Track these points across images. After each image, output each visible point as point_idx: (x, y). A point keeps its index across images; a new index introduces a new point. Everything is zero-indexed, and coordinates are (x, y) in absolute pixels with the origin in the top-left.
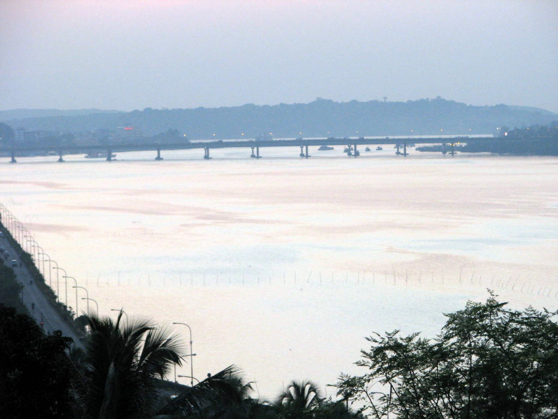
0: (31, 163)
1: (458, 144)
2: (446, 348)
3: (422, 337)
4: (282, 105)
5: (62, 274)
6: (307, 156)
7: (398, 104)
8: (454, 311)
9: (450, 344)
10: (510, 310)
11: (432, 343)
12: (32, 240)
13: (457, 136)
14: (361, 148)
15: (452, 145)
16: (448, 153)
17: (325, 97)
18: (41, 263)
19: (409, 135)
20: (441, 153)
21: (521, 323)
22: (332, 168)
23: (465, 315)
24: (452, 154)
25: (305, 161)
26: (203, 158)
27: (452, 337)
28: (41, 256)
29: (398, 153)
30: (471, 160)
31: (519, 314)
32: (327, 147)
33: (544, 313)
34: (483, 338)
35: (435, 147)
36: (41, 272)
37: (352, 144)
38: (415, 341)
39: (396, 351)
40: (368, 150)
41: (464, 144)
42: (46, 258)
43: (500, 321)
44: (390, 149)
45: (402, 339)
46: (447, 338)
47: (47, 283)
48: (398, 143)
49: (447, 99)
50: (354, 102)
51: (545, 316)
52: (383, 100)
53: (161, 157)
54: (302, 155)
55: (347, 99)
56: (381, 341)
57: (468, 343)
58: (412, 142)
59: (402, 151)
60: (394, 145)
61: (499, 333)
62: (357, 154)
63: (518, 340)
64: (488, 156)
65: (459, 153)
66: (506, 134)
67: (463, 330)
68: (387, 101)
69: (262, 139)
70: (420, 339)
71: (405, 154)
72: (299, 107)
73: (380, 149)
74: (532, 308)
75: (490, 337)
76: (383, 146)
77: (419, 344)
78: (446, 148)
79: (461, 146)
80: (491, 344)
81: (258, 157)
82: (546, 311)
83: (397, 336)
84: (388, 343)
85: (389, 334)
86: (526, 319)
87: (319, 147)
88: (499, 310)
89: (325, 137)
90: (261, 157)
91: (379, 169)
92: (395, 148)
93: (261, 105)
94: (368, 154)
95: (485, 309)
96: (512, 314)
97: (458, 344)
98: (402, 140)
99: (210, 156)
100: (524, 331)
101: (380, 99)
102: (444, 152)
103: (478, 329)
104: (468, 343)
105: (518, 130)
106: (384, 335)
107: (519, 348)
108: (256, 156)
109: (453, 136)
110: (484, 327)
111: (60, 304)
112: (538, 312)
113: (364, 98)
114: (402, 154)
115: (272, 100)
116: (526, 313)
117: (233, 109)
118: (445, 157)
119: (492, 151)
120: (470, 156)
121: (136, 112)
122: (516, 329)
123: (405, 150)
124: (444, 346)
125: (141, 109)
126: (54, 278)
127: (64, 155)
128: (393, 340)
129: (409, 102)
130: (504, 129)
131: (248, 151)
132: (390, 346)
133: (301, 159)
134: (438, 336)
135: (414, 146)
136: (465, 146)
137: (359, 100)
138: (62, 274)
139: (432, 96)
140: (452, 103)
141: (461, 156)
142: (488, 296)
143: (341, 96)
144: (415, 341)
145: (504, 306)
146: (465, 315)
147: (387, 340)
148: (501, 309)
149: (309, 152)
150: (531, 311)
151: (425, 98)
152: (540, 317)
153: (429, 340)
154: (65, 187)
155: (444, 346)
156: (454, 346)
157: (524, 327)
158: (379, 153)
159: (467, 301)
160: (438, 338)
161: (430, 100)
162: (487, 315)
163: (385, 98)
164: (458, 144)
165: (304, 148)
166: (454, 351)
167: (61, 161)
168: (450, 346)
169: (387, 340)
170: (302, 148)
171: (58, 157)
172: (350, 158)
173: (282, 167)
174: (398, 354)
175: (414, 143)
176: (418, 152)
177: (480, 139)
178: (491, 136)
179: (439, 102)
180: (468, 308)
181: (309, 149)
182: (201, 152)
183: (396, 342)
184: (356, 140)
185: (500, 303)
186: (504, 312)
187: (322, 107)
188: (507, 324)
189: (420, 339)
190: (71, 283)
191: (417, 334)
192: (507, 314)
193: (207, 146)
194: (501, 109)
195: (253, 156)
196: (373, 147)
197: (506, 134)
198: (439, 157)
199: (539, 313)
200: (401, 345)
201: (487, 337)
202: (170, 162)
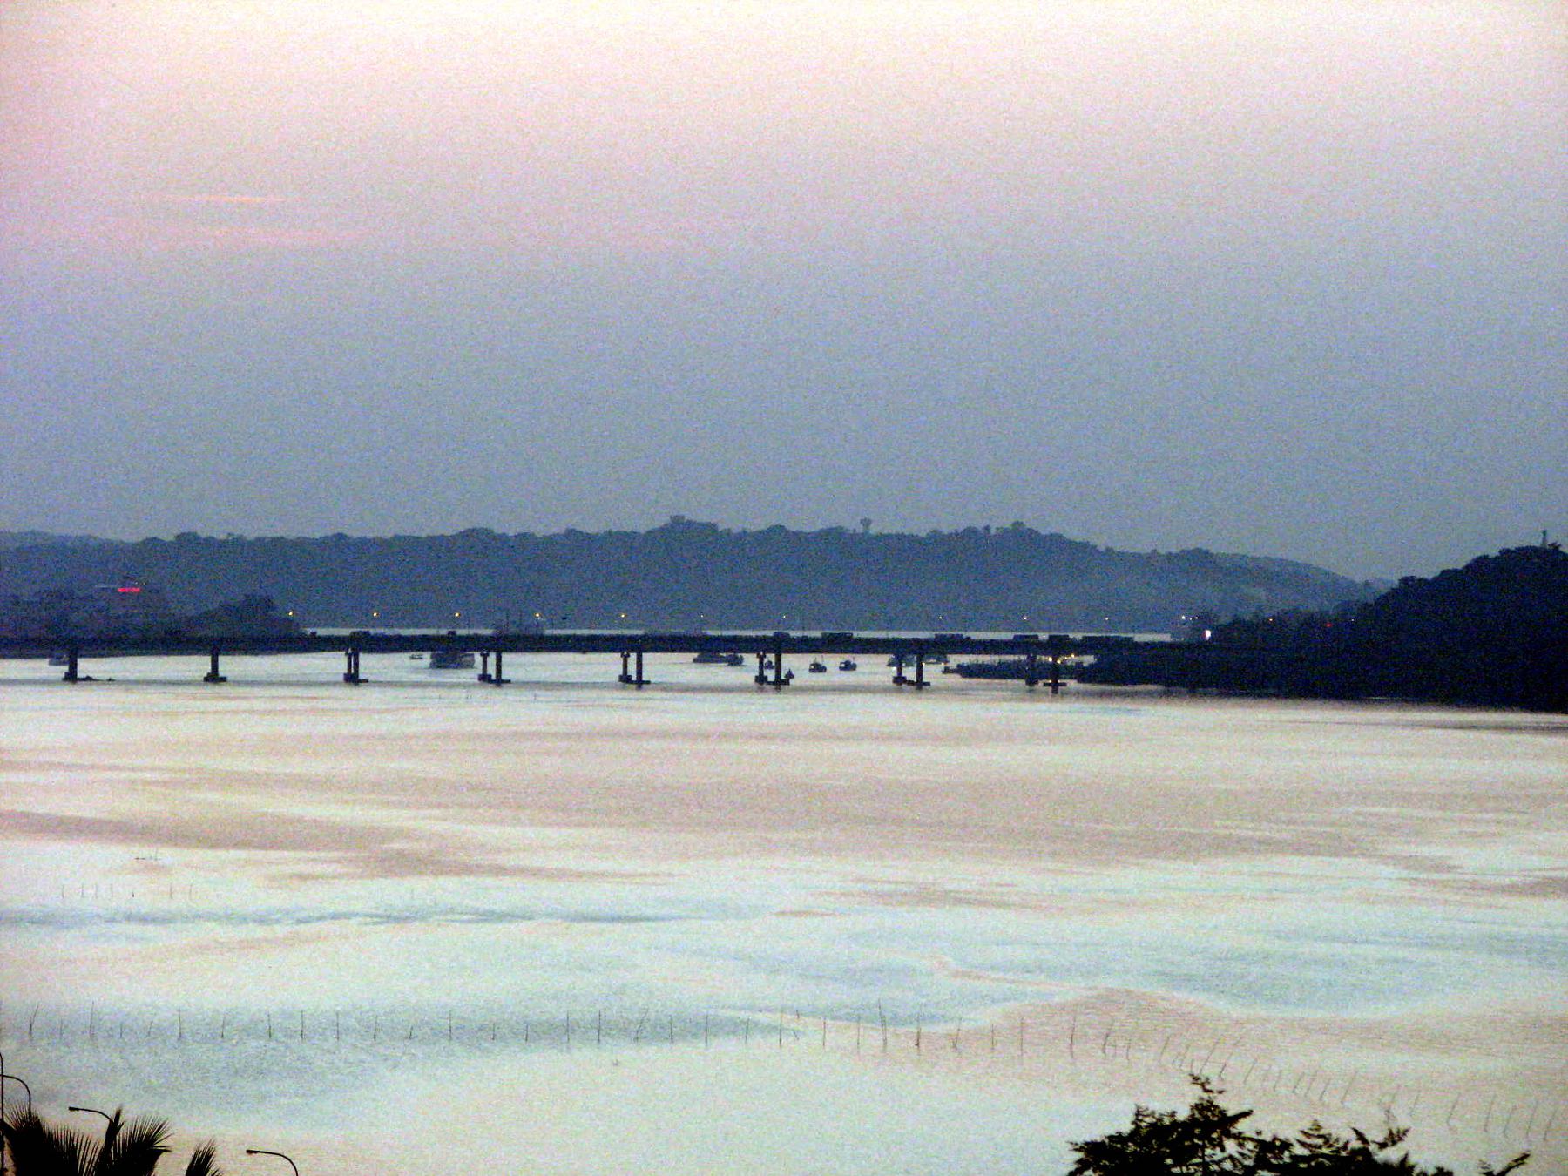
0: (1368, 724)
1: (1072, 659)
4: (571, 533)
10: (1259, 1133)
14: (795, 663)
15: (1055, 660)
16: (1041, 683)
20: (1022, 682)
22: (698, 714)
23: (1132, 1147)
25: (631, 694)
26: (341, 678)
29: (899, 680)
31: (1286, 1145)
33: (1356, 1144)
37: (769, 651)
40: (818, 668)
41: (1088, 660)
44: (876, 668)
48: (900, 651)
52: (860, 530)
53: (222, 672)
54: (625, 678)
55: (757, 523)
58: (939, 648)
59: (910, 673)
60: (887, 658)
64: (1150, 694)
65: (1072, 684)
66: (1208, 634)
68: (874, 530)
69: (513, 630)
71: (920, 684)
72: (623, 540)
73: (848, 667)
74: (1319, 1128)
76: (860, 660)
78: (1036, 665)
79: (1079, 664)
82: (1361, 1137)
87: (695, 655)
90: (224, 679)
91: (855, 722)
92: (890, 664)
94: (819, 679)
99: (361, 677)
101: (852, 525)
102: (1032, 682)
108: (634, 678)
112: (1337, 1140)
114: (911, 683)
115: (545, 526)
116: (1303, 1144)
119: (1167, 685)
120: (1101, 695)
123: (920, 674)
125: (169, 537)
130: (1205, 620)
133: (624, 688)
136: (1091, 666)
139: (1000, 520)
141: (1078, 694)
142: (1194, 1095)
143: (740, 514)
146: (1132, 1147)
149: (361, 670)
150: (1320, 1136)
151: (1008, 525)
152: (1344, 1154)
158: (848, 678)
161: (993, 531)
163: (866, 523)
165: (492, 658)
170: (625, 658)
172: (762, 690)
175: (944, 654)
176: (956, 679)
179: (1022, 539)
181: (361, 662)
182: (337, 663)
184: (486, 639)
185: (1230, 1113)
186: (1240, 1138)
187: (685, 546)
192: (1250, 1145)
193: (356, 645)
194: (1199, 561)
195: (485, 678)
196: (832, 661)
197: (1208, 634)
199: (1341, 1144)
202: (574, 694)
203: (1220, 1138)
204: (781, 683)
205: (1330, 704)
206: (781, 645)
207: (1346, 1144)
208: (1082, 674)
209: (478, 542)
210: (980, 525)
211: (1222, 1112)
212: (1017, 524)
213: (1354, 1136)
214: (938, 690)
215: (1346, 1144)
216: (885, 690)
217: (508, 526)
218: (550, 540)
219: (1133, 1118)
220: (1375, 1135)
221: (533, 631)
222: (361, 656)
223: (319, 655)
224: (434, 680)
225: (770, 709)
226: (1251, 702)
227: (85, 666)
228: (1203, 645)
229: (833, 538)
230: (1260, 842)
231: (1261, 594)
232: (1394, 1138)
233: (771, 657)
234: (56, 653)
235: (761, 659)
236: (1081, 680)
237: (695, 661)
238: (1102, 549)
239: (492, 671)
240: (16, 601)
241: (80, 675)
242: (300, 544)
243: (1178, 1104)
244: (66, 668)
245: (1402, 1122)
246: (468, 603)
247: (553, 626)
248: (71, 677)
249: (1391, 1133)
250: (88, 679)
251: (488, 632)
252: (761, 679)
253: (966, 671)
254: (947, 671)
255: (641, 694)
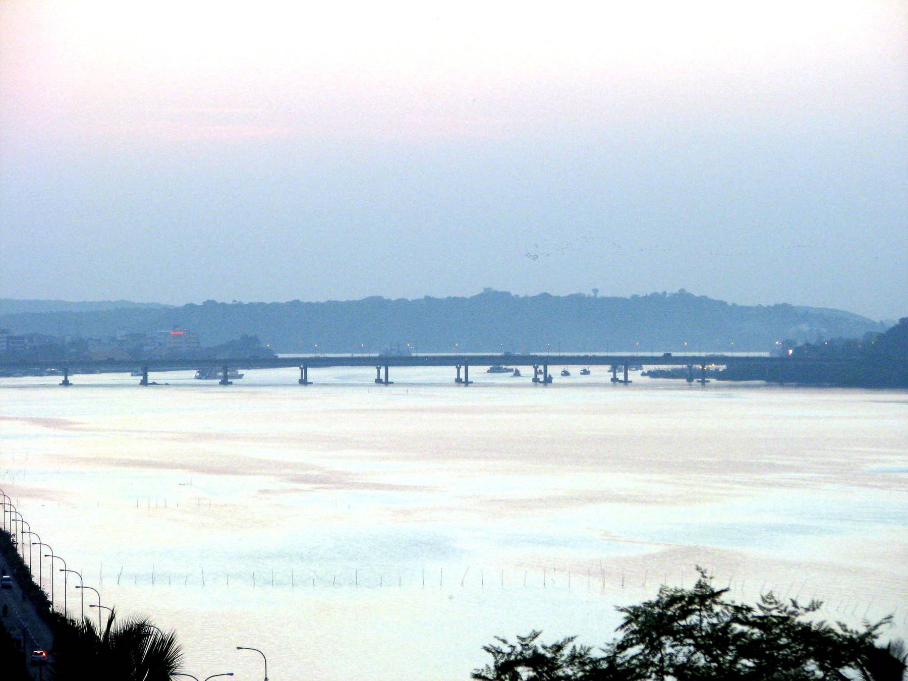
0: (14, 387)
1: (713, 367)
2: (623, 664)
3: (578, 643)
4: (428, 299)
5: (59, 565)
6: (467, 383)
7: (614, 300)
8: (638, 602)
9: (628, 658)
10: (733, 602)
11: (596, 654)
12: (13, 510)
13: (709, 354)
14: (554, 371)
16: (695, 380)
17: (499, 287)
18: (27, 549)
19: (633, 351)
20: (684, 381)
21: (753, 624)
22: (506, 404)
24: (703, 382)
25: (463, 390)
26: (297, 382)
27: (632, 645)
28: (26, 535)
29: (614, 380)
30: (734, 392)
31: (749, 610)
32: (499, 368)
33: (791, 608)
34: (686, 649)
35: (674, 370)
36: (27, 562)
38: (566, 652)
39: (535, 670)
40: (566, 374)
41: (722, 368)
42: (34, 539)
43: (715, 621)
44: (602, 373)
45: (544, 647)
46: (622, 647)
47: (36, 580)
48: (616, 363)
49: (697, 295)
50: (546, 296)
51: (793, 613)
52: (592, 294)
54: (458, 380)
55: (533, 292)
56: (508, 650)
57: (659, 655)
58: (637, 362)
59: (620, 376)
60: (608, 367)
61: (717, 640)
62: (548, 381)
63: (744, 652)
64: (758, 387)
65: (713, 381)
66: (791, 352)
67: (650, 636)
68: (599, 295)
69: (394, 353)
70: (574, 647)
71: (626, 382)
72: (455, 303)
73: (585, 372)
75: (698, 647)
76: (592, 369)
77: (573, 657)
78: (694, 373)
79: (717, 370)
80: (701, 660)
81: (387, 383)
82: (795, 604)
83: (537, 643)
84: (521, 653)
85: (523, 639)
86: (760, 618)
87: (488, 367)
88: (716, 603)
89: (501, 351)
91: (582, 404)
93: (393, 299)
94: (566, 380)
95: (691, 600)
96: (738, 609)
97: (641, 657)
98: (621, 358)
99: (309, 381)
100: (755, 637)
101: (588, 292)
102: (690, 380)
103: (678, 632)
104: (659, 655)
105: (808, 345)
106: (514, 641)
107: (746, 666)
109: (703, 354)
110: (688, 631)
111: (57, 615)
113: (560, 290)
114: (621, 381)
115: (413, 292)
116: (761, 607)
117: (350, 304)
118: (690, 388)
119: (767, 380)
120: (730, 387)
121: (191, 307)
122: (743, 634)
124: (619, 661)
126: (46, 574)
127: (72, 374)
128: (529, 649)
129: (635, 297)
130: (788, 344)
131: (371, 372)
132: (525, 658)
134: (608, 645)
135: (641, 369)
137: (555, 293)
138: (59, 565)
139: (672, 289)
140: (703, 300)
141: (717, 387)
144: (566, 652)
145: (724, 594)
146: (657, 610)
147: (519, 648)
148: (718, 600)
153: (589, 649)
154: (77, 426)
155: (619, 661)
156: (635, 661)
157: (756, 630)
159: (660, 586)
160: (609, 648)
162: (696, 610)
163: (596, 291)
164: (713, 367)
165: (463, 369)
166: (634, 669)
167: (66, 383)
168: (629, 662)
169: (519, 648)
171: (61, 379)
173: (426, 399)
174: (538, 673)
175: (641, 364)
176: (647, 379)
177: (747, 359)
178: (766, 354)
179: (684, 299)
180: (661, 598)
182: (294, 373)
183: (535, 652)
185: (716, 591)
188: (728, 624)
189: (574, 647)
190: (73, 580)
191: (571, 639)
193: (305, 364)
194: (784, 311)
195: (378, 381)
198: (680, 388)
200: (543, 656)
201: (692, 648)
203: (710, 605)
204: (548, 381)
205: (863, 391)
206: (548, 361)
207: (786, 608)
208: (719, 376)
209: (376, 304)
210: (660, 291)
211: (712, 590)
212: (682, 290)
213: (790, 604)
214: (559, 386)
215: (786, 608)
216: (605, 385)
217: (392, 294)
218: (416, 302)
219: (657, 592)
220: (804, 603)
221: (405, 355)
222: (470, 367)
223: (176, 372)
224: (488, 381)
225: (543, 395)
226: (813, 390)
227: (152, 376)
228: (789, 358)
229: (576, 300)
230: (784, 466)
231: (805, 327)
232: (814, 607)
233: (541, 368)
234: (136, 369)
235: (536, 368)
236: (719, 378)
237: (488, 372)
238: (730, 304)
239: (382, 377)
240: (113, 339)
241: (149, 381)
242: (276, 306)
243: (688, 586)
244: (141, 378)
245: (713, 575)
246: (382, 337)
247: (417, 351)
248: (144, 383)
249: (813, 603)
250: (154, 383)
251: (377, 355)
252: (536, 380)
253: (652, 374)
254: (643, 374)
255: (467, 389)
